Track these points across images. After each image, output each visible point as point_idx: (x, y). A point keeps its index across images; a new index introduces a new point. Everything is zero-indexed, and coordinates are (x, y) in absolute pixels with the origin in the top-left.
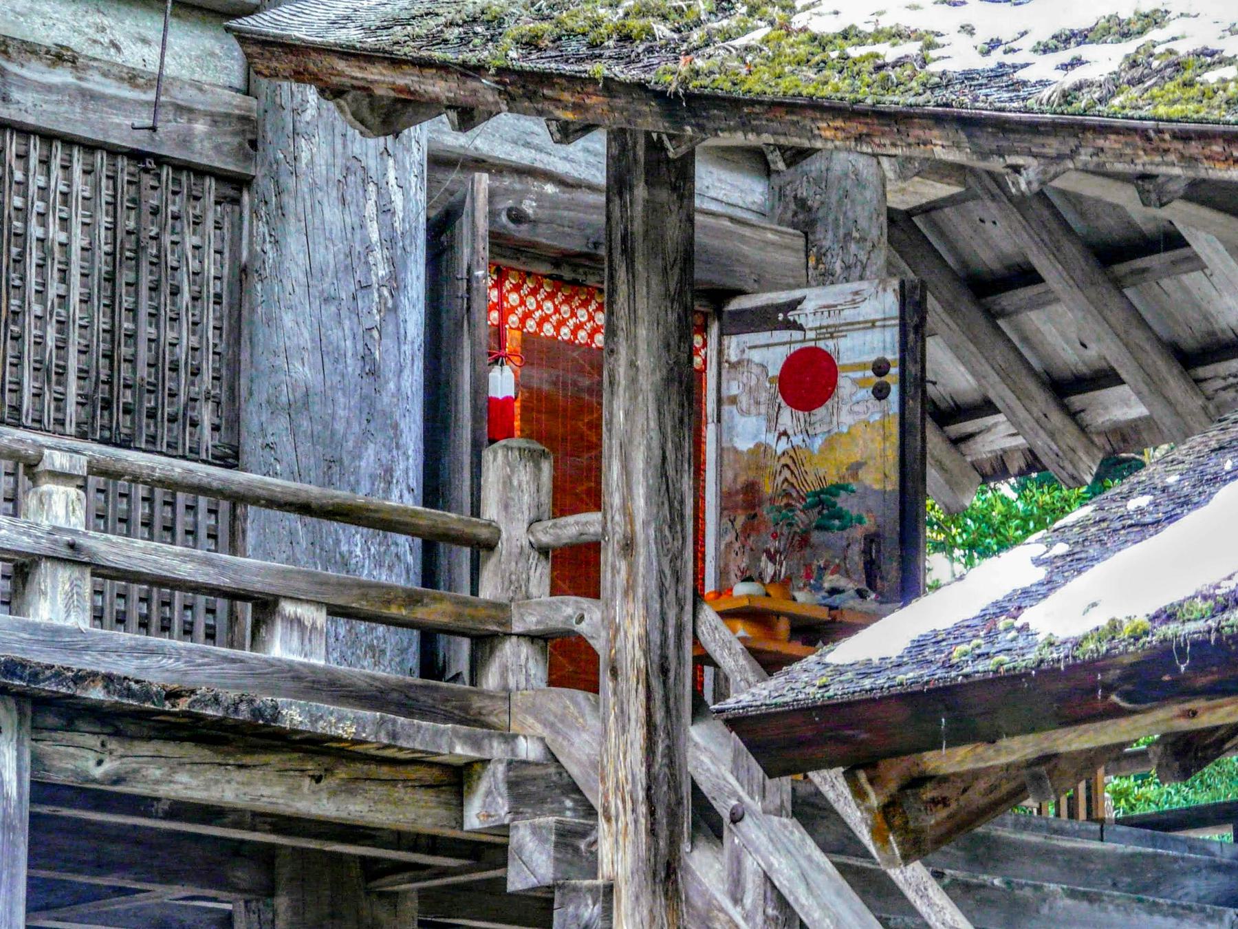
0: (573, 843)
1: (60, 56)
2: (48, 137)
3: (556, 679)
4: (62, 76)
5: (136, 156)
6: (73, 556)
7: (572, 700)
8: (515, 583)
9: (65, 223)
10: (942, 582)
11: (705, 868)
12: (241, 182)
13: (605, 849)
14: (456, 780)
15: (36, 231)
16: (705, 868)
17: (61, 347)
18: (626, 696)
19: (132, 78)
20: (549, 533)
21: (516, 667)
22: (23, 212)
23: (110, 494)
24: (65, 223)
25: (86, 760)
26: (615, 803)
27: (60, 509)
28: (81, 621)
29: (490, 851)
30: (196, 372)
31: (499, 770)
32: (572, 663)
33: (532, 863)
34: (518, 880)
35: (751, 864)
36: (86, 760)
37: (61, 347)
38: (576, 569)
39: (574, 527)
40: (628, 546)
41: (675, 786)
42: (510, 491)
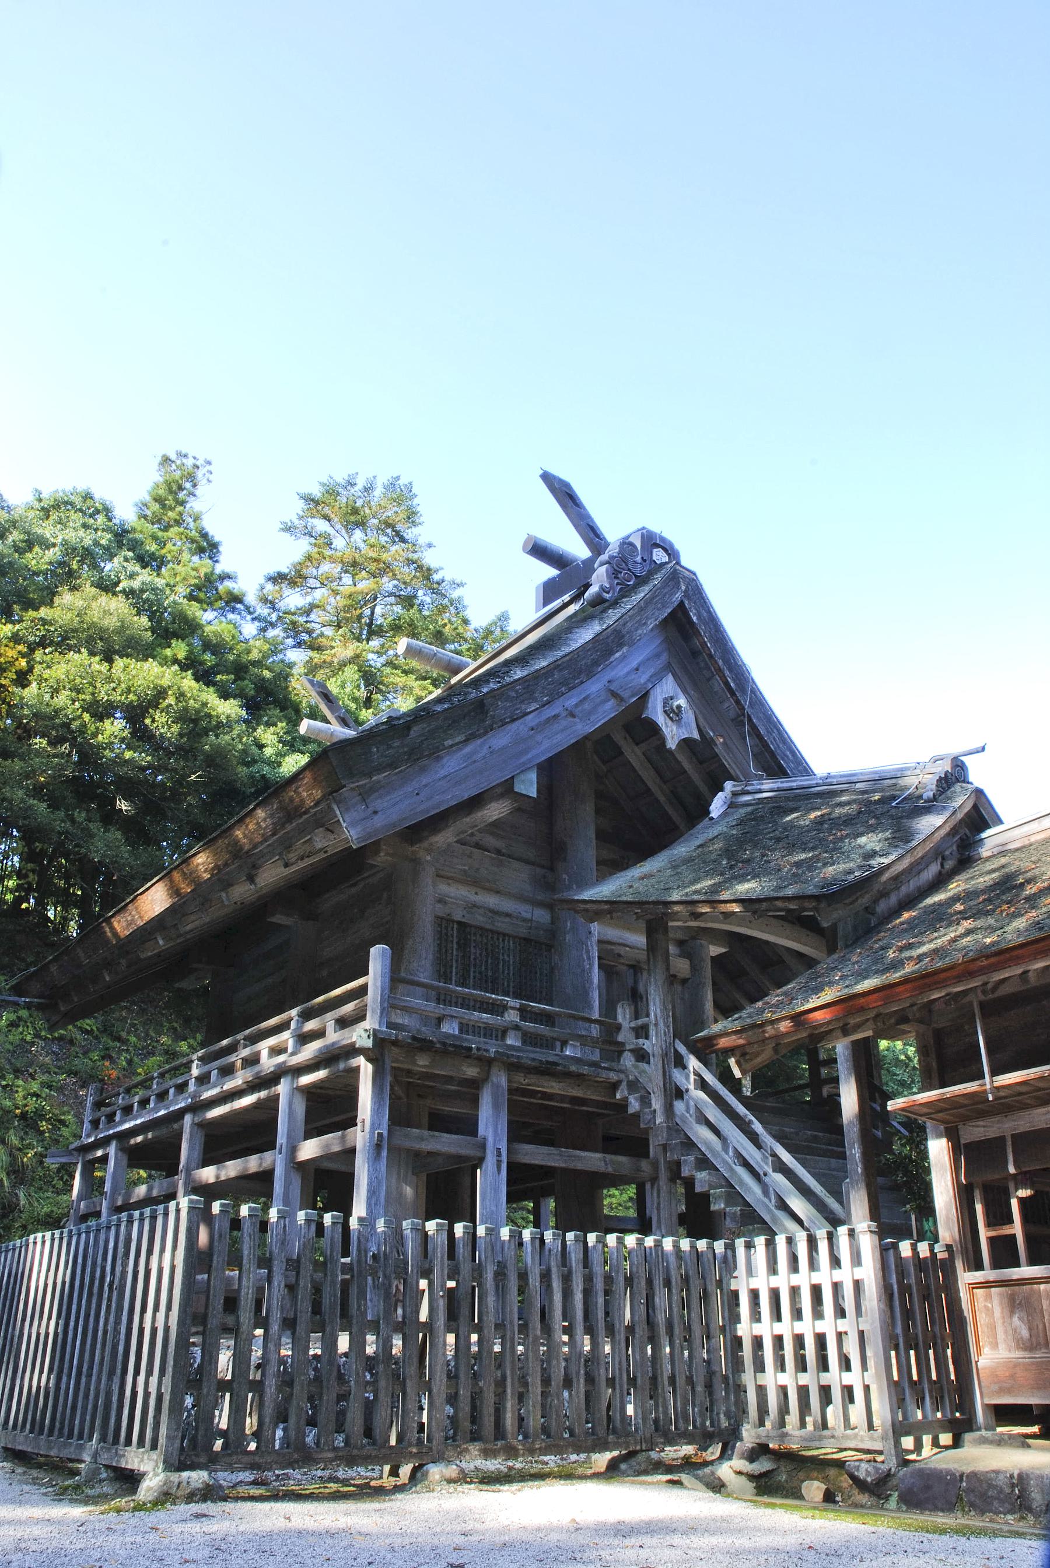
0: (645, 1100)
1: (508, 915)
2: (504, 935)
3: (638, 1060)
4: (507, 920)
5: (525, 939)
6: (517, 1028)
7: (643, 1065)
8: (625, 1036)
9: (508, 956)
10: (750, 1279)
11: (679, 1106)
12: (549, 947)
13: (653, 1102)
14: (615, 1086)
15: (501, 957)
16: (679, 1106)
17: (508, 986)
18: (656, 1062)
19: (525, 920)
20: (633, 1025)
21: (628, 1060)
22: (498, 953)
23: (523, 1012)
24: (508, 956)
25: (522, 1080)
26: (655, 1089)
27: (512, 1016)
28: (518, 1044)
29: (623, 1105)
30: (541, 992)
31: (624, 1084)
32: (642, 1056)
33: (634, 1105)
34: (631, 1110)
35: (692, 1103)
36: (522, 1080)
37: (508, 986)
38: (642, 1032)
39: (640, 1022)
40: (656, 1025)
41: (670, 1084)
42: (623, 1015)
